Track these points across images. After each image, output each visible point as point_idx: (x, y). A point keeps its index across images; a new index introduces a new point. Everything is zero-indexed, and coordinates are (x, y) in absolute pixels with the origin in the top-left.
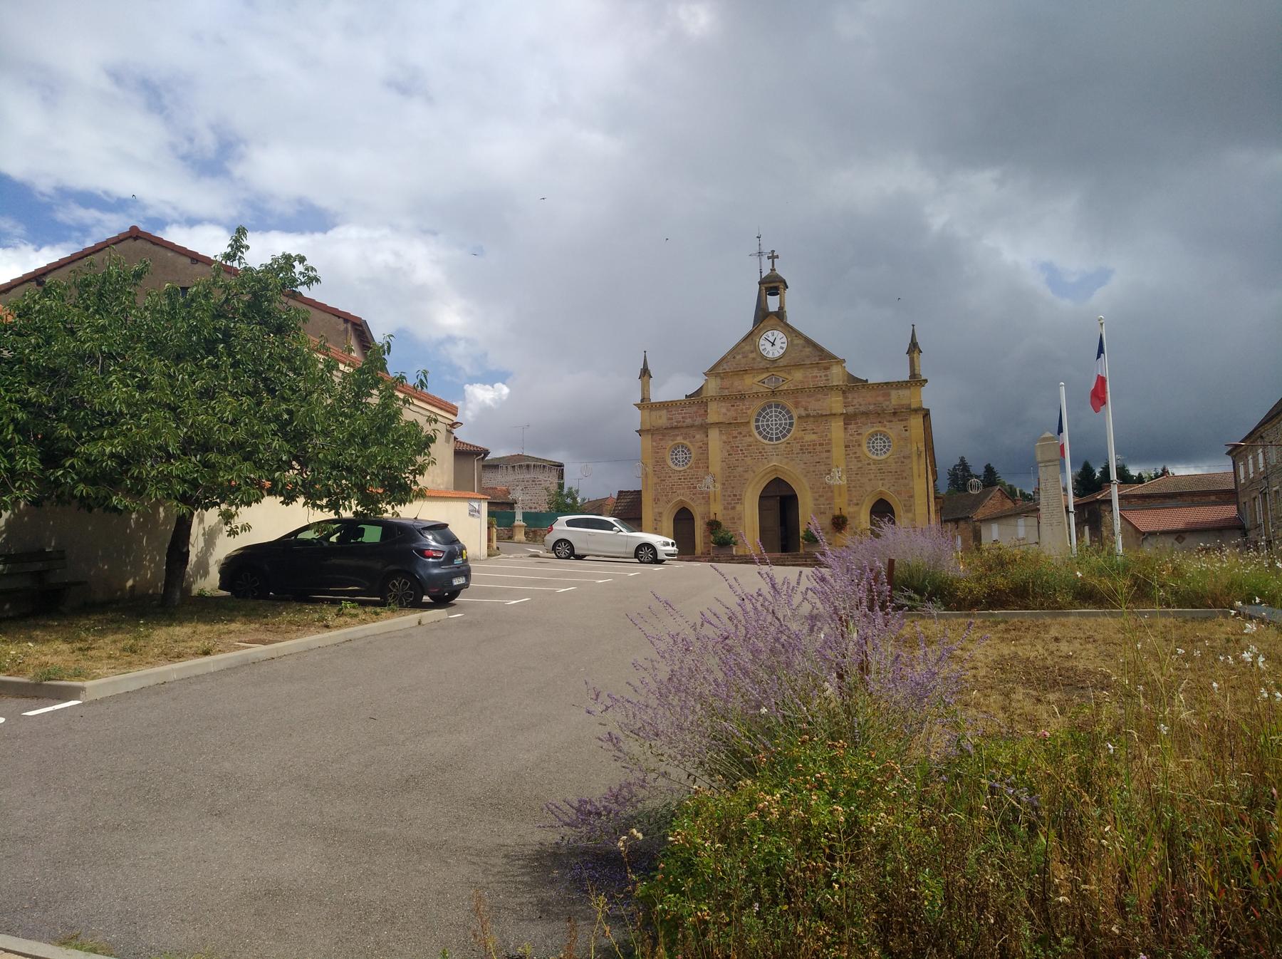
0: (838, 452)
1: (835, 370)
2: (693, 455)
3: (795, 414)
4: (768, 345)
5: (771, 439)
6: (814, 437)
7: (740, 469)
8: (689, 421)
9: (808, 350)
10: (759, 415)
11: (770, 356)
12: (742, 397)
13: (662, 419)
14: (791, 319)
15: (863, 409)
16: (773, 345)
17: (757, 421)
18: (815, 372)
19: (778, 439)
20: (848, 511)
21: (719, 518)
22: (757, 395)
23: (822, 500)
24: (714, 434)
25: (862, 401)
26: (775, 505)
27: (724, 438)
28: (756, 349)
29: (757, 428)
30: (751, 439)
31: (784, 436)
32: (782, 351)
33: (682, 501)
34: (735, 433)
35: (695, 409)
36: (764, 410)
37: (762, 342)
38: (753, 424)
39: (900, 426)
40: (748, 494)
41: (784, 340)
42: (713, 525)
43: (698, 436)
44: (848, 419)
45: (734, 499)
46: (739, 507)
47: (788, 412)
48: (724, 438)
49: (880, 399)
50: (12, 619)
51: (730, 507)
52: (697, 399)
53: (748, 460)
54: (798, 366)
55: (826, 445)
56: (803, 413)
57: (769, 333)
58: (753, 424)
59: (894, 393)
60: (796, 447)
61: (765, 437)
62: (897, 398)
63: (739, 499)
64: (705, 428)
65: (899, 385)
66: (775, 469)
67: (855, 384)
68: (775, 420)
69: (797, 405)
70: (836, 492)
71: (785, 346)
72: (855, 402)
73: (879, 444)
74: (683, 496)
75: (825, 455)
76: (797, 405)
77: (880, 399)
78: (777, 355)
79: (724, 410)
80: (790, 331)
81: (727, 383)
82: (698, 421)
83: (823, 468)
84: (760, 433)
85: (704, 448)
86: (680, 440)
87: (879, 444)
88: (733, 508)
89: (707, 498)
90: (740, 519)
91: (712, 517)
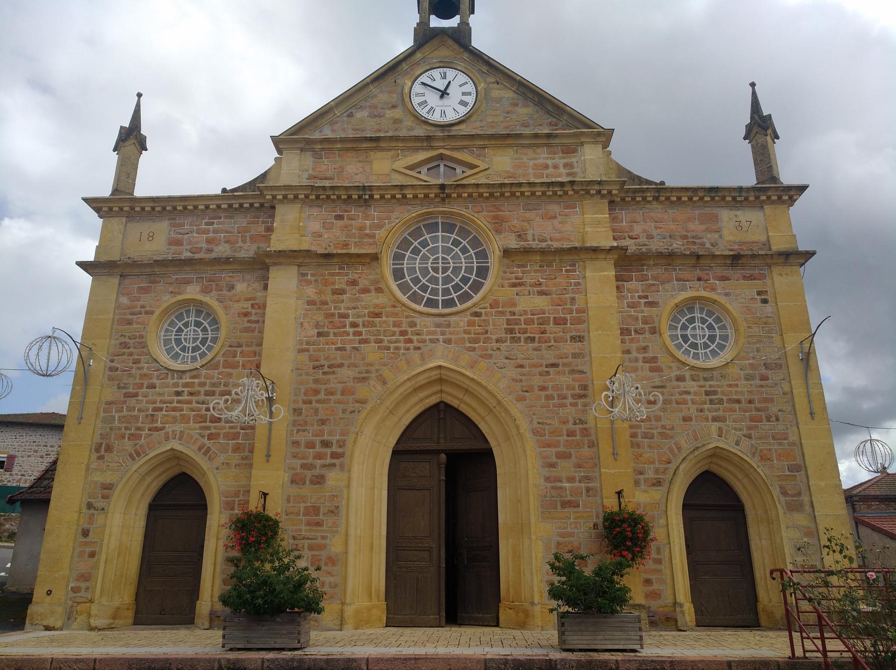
0: (604, 344)
1: (590, 153)
2: (223, 333)
3: (495, 246)
4: (432, 98)
5: (431, 303)
6: (541, 302)
7: (346, 373)
8: (222, 250)
9: (525, 111)
10: (404, 244)
11: (436, 117)
12: (363, 196)
13: (153, 241)
14: (478, 42)
15: (656, 245)
16: (445, 97)
17: (398, 257)
18: (543, 156)
19: (449, 303)
20: (639, 499)
21: (274, 509)
22: (398, 195)
23: (566, 468)
24: (284, 282)
25: (650, 229)
26: (431, 475)
27: (310, 292)
28: (404, 101)
29: (398, 274)
30: (381, 299)
31: (465, 297)
32: (463, 111)
33: (175, 456)
34: (340, 282)
35: (241, 221)
36: (416, 233)
37: (417, 88)
38: (387, 267)
39: (747, 290)
40: (363, 440)
41: (470, 87)
42: (255, 531)
43: (241, 287)
44: (627, 262)
45: (323, 456)
46: (333, 478)
47: (475, 243)
48: (310, 292)
49: (696, 227)
50: (410, 659)
51: (309, 477)
52: (254, 200)
53: (371, 353)
54: (505, 139)
55: (573, 323)
56: (513, 243)
57: (436, 73)
58: (387, 267)
59: (726, 216)
60: (497, 325)
61: (415, 298)
62: (735, 228)
63: (337, 455)
64: (261, 265)
65: (735, 197)
66: (441, 378)
67: (630, 192)
68: (441, 253)
69: (499, 224)
70: (605, 449)
71: (471, 100)
72: (637, 229)
73: (699, 332)
74: (182, 440)
75: (569, 348)
76: (499, 224)
77: (696, 227)
78: (451, 117)
79: (315, 226)
80: (485, 66)
81: (328, 166)
82: (247, 250)
83: (565, 380)
84: (404, 288)
85: (254, 317)
86: (192, 292)
87: (699, 332)
88: (319, 480)
89: (244, 443)
90: (334, 512)
91: (254, 505)
